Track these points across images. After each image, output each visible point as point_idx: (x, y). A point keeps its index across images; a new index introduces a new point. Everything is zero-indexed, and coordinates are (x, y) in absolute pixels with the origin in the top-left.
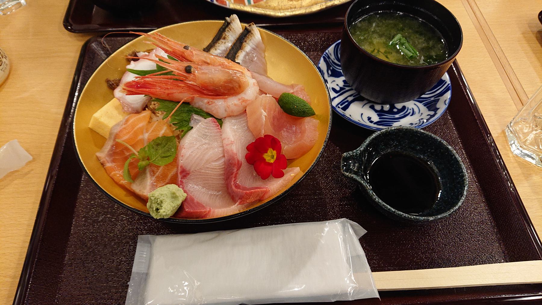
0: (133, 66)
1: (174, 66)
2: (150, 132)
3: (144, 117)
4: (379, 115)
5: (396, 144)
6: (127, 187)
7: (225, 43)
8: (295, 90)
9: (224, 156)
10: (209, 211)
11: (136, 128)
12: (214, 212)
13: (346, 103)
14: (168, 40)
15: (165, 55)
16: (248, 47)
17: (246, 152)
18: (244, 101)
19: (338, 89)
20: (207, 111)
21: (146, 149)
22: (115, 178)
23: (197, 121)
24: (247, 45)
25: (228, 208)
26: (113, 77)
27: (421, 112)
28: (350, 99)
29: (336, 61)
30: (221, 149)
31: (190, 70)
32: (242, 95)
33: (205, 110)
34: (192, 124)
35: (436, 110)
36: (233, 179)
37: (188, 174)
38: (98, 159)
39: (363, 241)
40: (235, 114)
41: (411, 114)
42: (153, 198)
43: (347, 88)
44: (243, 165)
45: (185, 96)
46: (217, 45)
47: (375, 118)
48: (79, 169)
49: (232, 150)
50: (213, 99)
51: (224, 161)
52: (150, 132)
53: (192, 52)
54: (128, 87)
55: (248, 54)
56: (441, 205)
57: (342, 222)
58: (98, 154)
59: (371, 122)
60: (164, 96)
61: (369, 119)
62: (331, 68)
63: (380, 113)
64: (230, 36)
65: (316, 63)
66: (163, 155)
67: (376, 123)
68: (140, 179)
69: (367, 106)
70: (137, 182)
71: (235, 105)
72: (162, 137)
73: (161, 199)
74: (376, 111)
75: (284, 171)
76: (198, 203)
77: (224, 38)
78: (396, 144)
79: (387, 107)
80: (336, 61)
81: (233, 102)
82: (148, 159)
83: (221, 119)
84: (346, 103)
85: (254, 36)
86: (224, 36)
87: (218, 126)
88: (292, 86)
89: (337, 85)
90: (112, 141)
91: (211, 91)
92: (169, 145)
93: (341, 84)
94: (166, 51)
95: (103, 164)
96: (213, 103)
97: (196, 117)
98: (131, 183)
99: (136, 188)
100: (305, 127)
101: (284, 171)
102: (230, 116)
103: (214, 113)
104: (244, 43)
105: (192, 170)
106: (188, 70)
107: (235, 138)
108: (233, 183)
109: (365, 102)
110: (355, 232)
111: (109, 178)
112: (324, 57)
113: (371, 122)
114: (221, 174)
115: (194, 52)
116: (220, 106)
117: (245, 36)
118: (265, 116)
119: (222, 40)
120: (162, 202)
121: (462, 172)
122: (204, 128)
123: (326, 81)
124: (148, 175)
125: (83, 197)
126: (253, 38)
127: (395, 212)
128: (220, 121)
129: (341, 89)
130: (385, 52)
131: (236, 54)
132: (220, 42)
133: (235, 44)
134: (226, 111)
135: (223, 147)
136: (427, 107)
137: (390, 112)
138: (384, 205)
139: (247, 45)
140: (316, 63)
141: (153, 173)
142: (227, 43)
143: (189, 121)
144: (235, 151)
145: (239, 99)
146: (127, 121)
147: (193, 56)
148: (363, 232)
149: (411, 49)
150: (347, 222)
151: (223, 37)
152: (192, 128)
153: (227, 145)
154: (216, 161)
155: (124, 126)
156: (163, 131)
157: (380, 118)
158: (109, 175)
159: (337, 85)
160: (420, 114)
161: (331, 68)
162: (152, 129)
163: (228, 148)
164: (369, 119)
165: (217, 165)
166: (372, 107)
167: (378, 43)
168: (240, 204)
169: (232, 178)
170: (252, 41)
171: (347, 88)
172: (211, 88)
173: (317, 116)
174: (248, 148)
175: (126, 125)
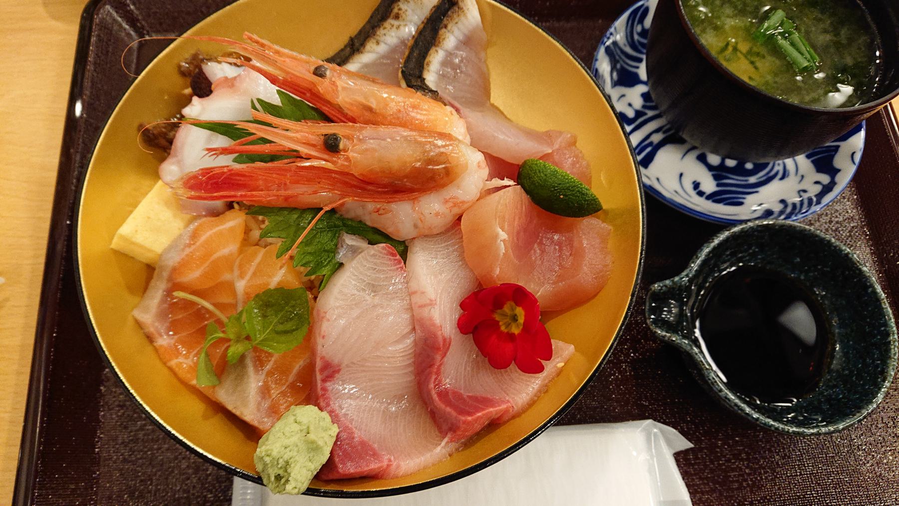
0: (196, 109)
1: (298, 135)
2: (248, 277)
3: (232, 229)
4: (716, 177)
5: (754, 252)
6: (209, 393)
7: (398, 27)
8: (556, 146)
9: (414, 329)
10: (388, 466)
11: (216, 256)
12: (398, 467)
13: (649, 149)
14: (277, 52)
15: (270, 93)
16: (450, 39)
17: (457, 313)
18: (455, 205)
19: (631, 114)
20: (375, 225)
21: (244, 317)
22: (181, 374)
23: (355, 251)
24: (448, 34)
25: (428, 455)
26: (155, 121)
27: (801, 172)
28: (656, 138)
29: (628, 50)
30: (406, 316)
31: (337, 146)
32: (451, 192)
33: (369, 223)
34: (341, 256)
35: (833, 172)
36: (434, 377)
37: (338, 371)
38: (139, 325)
39: (680, 458)
40: (435, 231)
41: (780, 176)
42: (267, 459)
43: (650, 113)
44: (452, 343)
45: (325, 196)
46: (380, 32)
47: (709, 185)
48: (96, 359)
49: (431, 319)
50: (389, 202)
51: (415, 341)
52: (248, 277)
53: (334, 84)
54: (191, 188)
55: (450, 54)
56: (835, 386)
57: (644, 429)
58: (138, 314)
59: (701, 194)
60: (281, 203)
61: (696, 185)
62: (618, 66)
63: (719, 173)
64: (409, 12)
65: (588, 60)
66: (281, 328)
67: (710, 197)
68: (232, 377)
69: (692, 157)
70: (228, 383)
71: (437, 214)
72: (276, 289)
73: (286, 457)
74: (710, 168)
75: (544, 362)
76: (363, 443)
77: (397, 17)
78: (754, 252)
79: (731, 163)
80: (628, 50)
81: (433, 208)
82: (248, 338)
83: (404, 242)
84: (649, 149)
85: (465, 15)
86: (396, 10)
87: (400, 262)
88: (547, 137)
89: (630, 105)
90: (165, 282)
91: (385, 186)
92: (292, 310)
93: (638, 103)
94: (273, 80)
95: (150, 339)
96: (387, 211)
97: (350, 240)
98: (214, 387)
99: (224, 396)
100: (581, 243)
101: (544, 362)
102: (428, 236)
103: (390, 230)
104: (442, 31)
105: (346, 362)
106: (331, 145)
107: (436, 283)
108: (432, 385)
109: (686, 146)
110: (669, 442)
111: (166, 371)
112: (608, 50)
113: (701, 194)
114: (406, 373)
115: (339, 83)
116: (403, 216)
117: (445, 14)
118: (504, 241)
119: (391, 21)
120: (287, 463)
121: (886, 324)
122: (369, 269)
123: (608, 98)
124: (251, 369)
125: (109, 417)
126: (462, 18)
127: (757, 419)
128: (402, 250)
129: (639, 114)
130: (750, 52)
131: (424, 57)
132: (387, 24)
133: (421, 33)
134: (416, 226)
135: (411, 309)
136: (813, 162)
137: (740, 170)
138: (736, 405)
139: (448, 34)
140: (588, 60)
141: (260, 363)
142: (402, 28)
143: (335, 251)
144: (438, 320)
145: (446, 201)
146: (194, 236)
147: (335, 91)
148: (684, 444)
149: (803, 48)
150: (656, 427)
151: (393, 14)
152: (341, 265)
153: (421, 307)
154: (398, 342)
155: (188, 251)
156: (279, 276)
157: (718, 185)
158: (165, 364)
159: (630, 105)
160: (799, 178)
161: (618, 66)
162: (252, 269)
163: (425, 313)
164: (696, 185)
165: (398, 351)
166: (702, 158)
167: (734, 28)
168: (451, 441)
169: (430, 373)
170: (460, 25)
171: (650, 113)
172: (386, 181)
173: (606, 212)
174: (463, 305)
175: (193, 247)
